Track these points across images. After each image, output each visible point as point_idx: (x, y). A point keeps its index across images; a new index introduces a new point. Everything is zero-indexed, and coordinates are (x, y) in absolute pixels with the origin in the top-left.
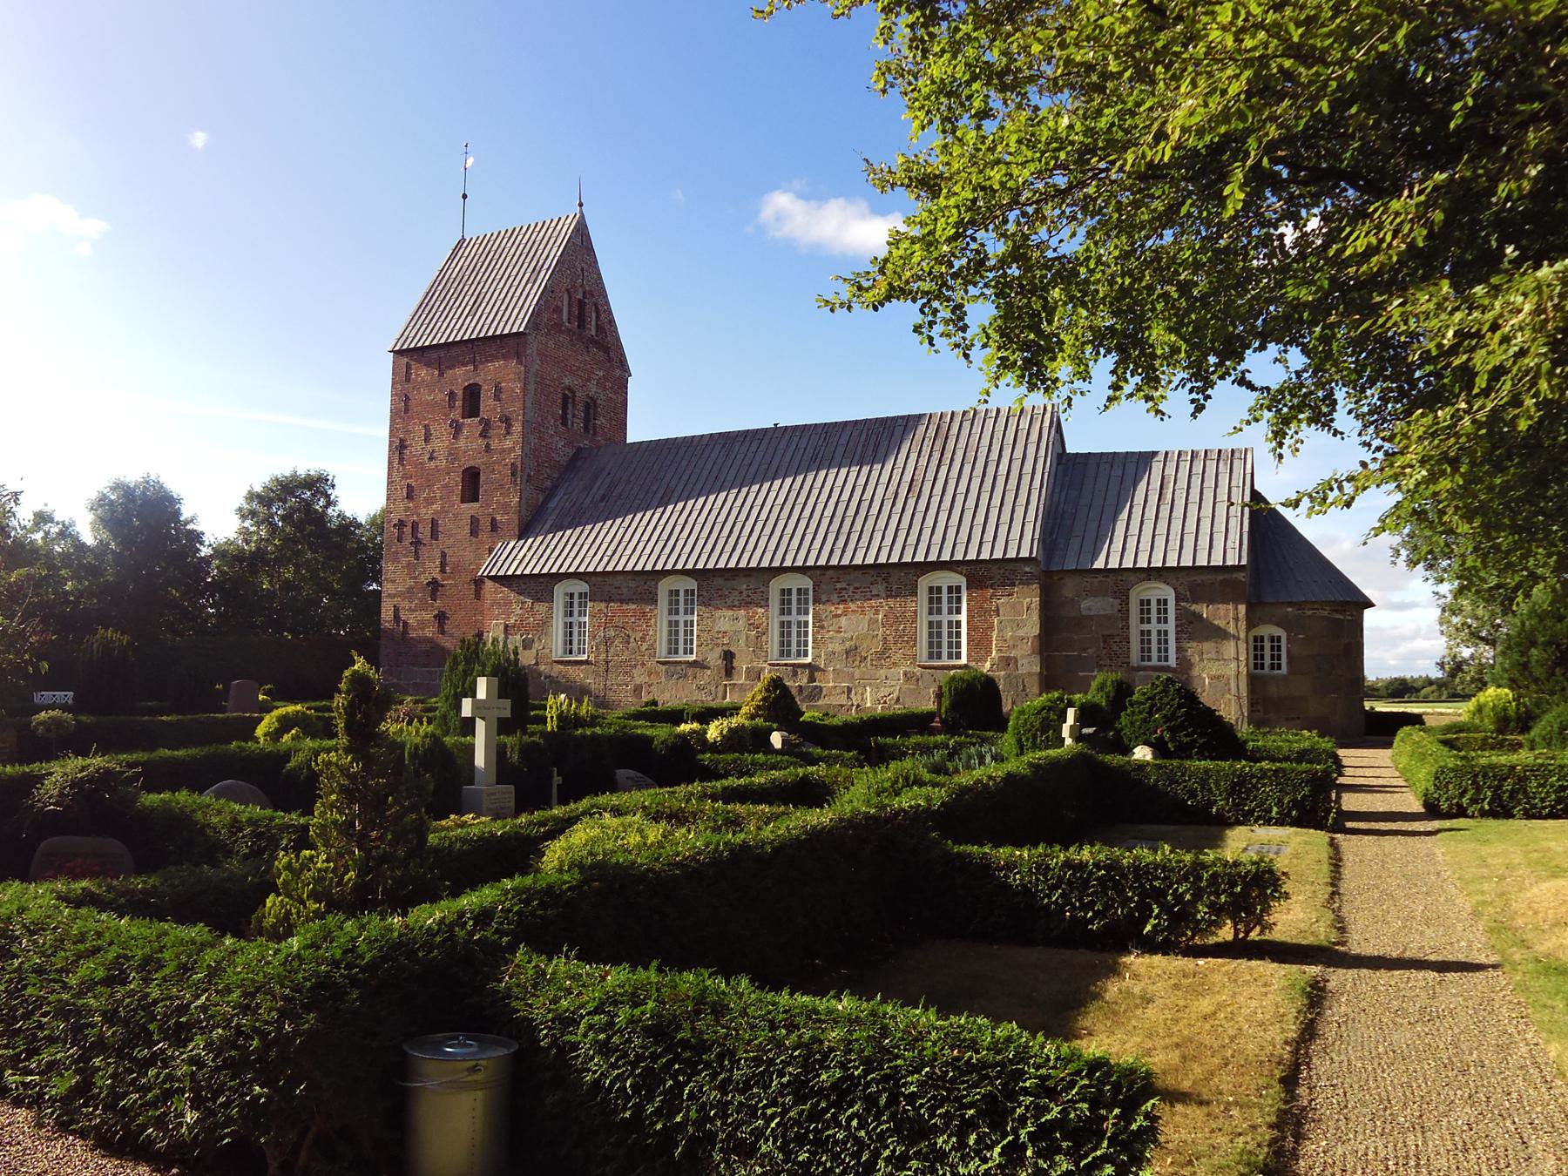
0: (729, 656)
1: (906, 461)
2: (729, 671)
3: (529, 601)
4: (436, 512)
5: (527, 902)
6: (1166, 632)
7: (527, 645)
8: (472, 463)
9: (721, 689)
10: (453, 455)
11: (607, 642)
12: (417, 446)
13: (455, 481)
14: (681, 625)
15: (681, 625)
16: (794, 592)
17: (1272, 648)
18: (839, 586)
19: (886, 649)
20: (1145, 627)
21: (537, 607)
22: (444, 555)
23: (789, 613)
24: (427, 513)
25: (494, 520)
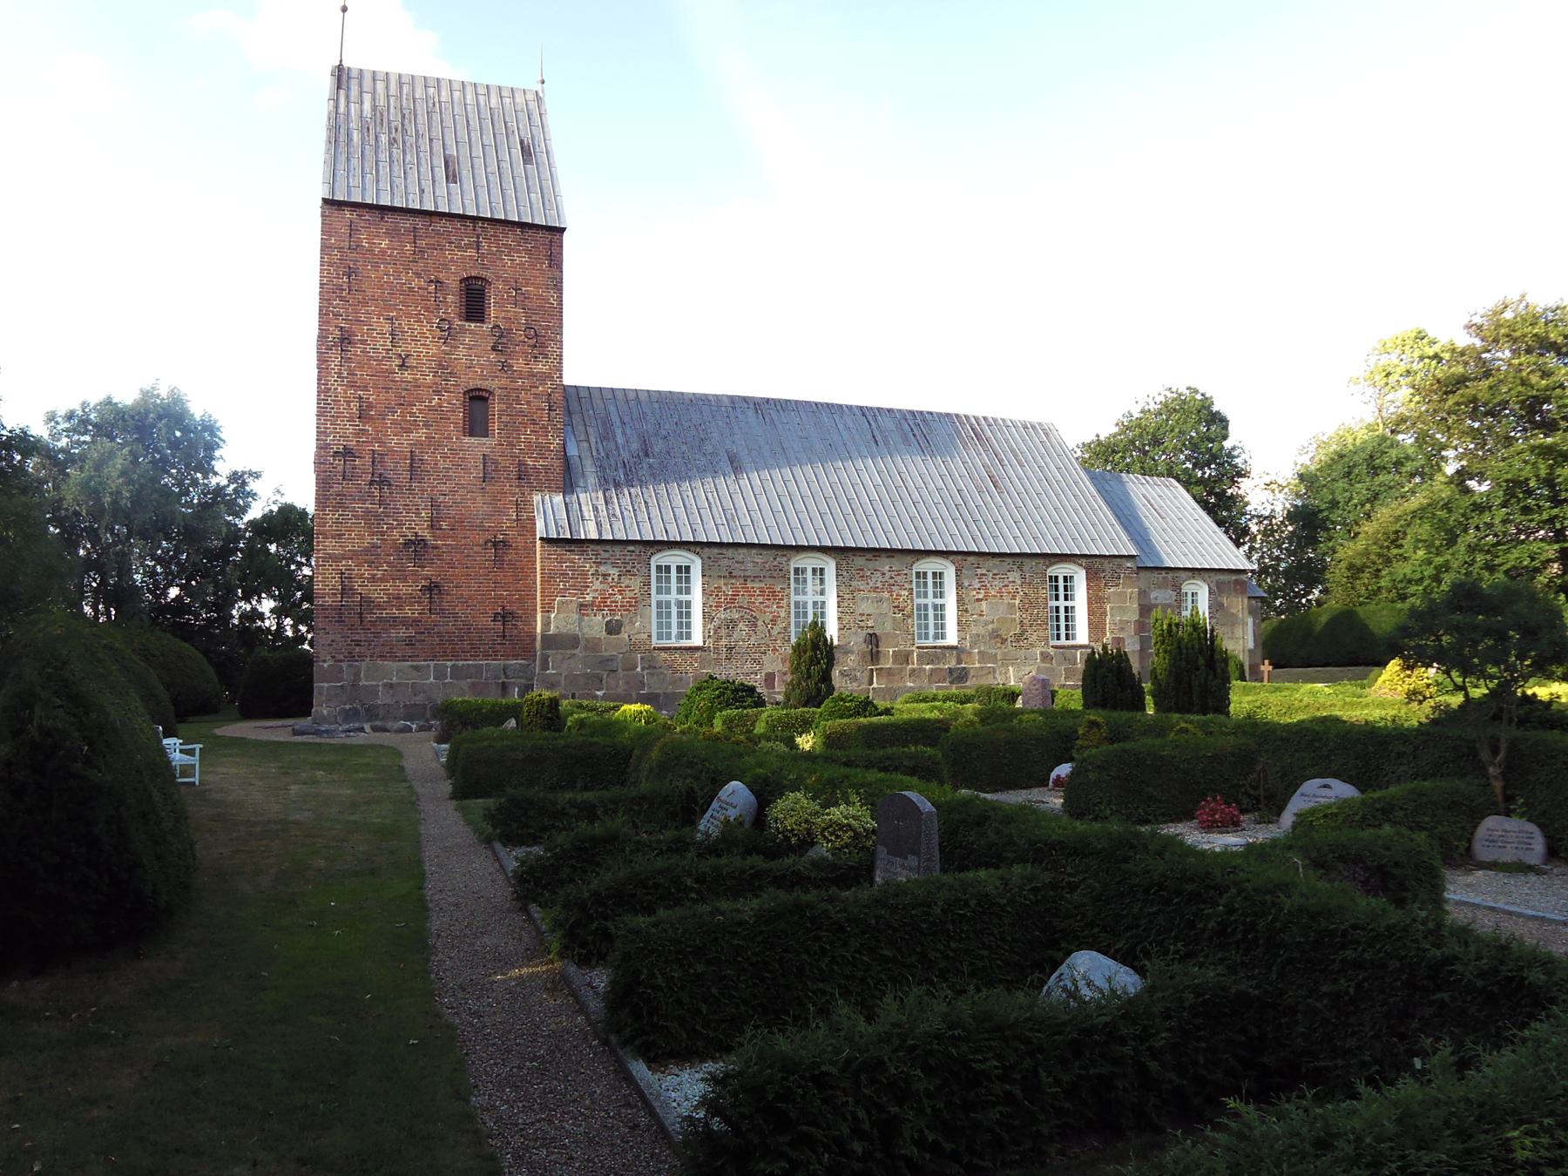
0: (873, 639)
1: (963, 465)
2: (875, 656)
3: (614, 572)
4: (419, 444)
5: (951, 1027)
6: (688, 604)
7: (613, 628)
8: (479, 384)
9: (867, 674)
10: (444, 367)
11: (731, 625)
12: (376, 336)
13: (453, 402)
14: (1062, 610)
15: (1062, 610)
16: (930, 576)
17: (936, 617)
18: (979, 571)
19: (1023, 632)
20: (664, 597)
21: (626, 581)
22: (434, 505)
23: (668, 592)
24: (399, 443)
25: (521, 463)
